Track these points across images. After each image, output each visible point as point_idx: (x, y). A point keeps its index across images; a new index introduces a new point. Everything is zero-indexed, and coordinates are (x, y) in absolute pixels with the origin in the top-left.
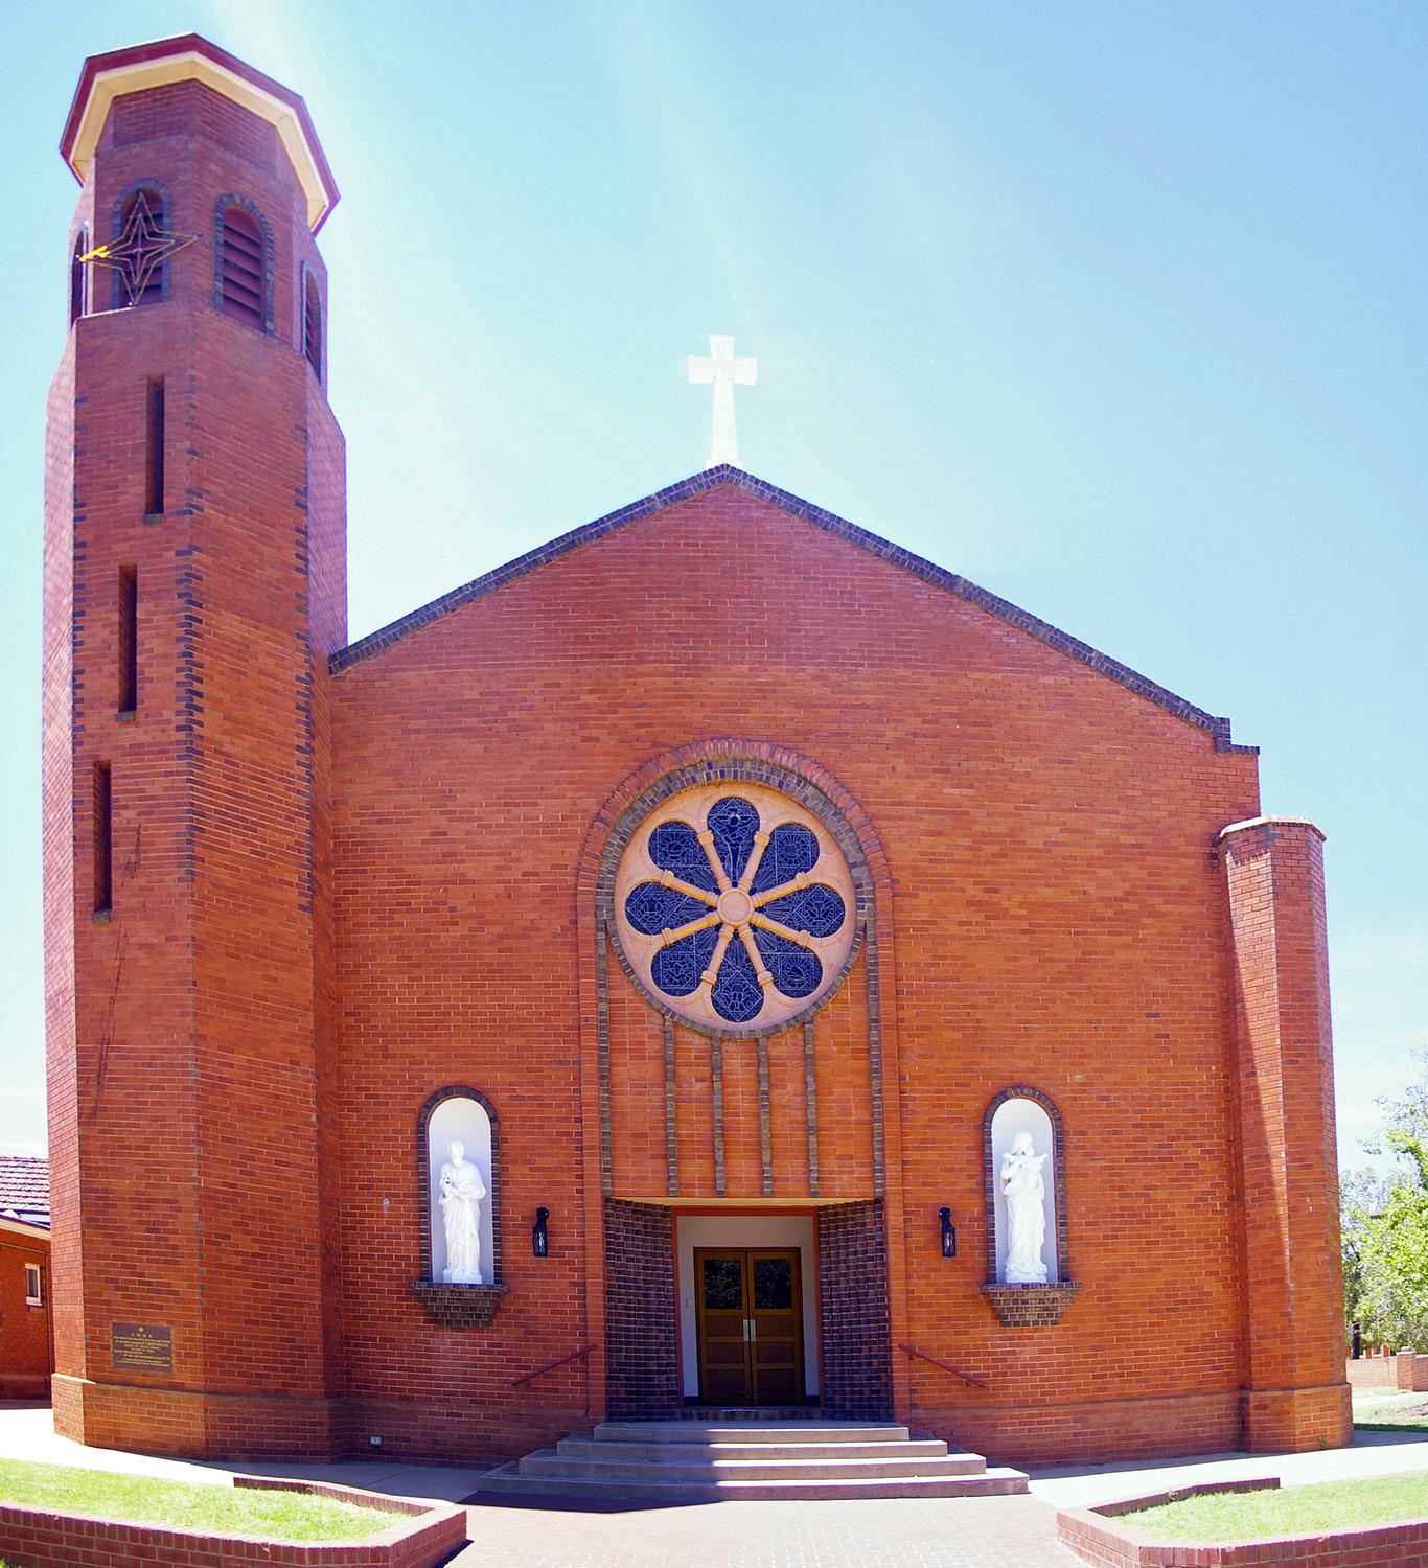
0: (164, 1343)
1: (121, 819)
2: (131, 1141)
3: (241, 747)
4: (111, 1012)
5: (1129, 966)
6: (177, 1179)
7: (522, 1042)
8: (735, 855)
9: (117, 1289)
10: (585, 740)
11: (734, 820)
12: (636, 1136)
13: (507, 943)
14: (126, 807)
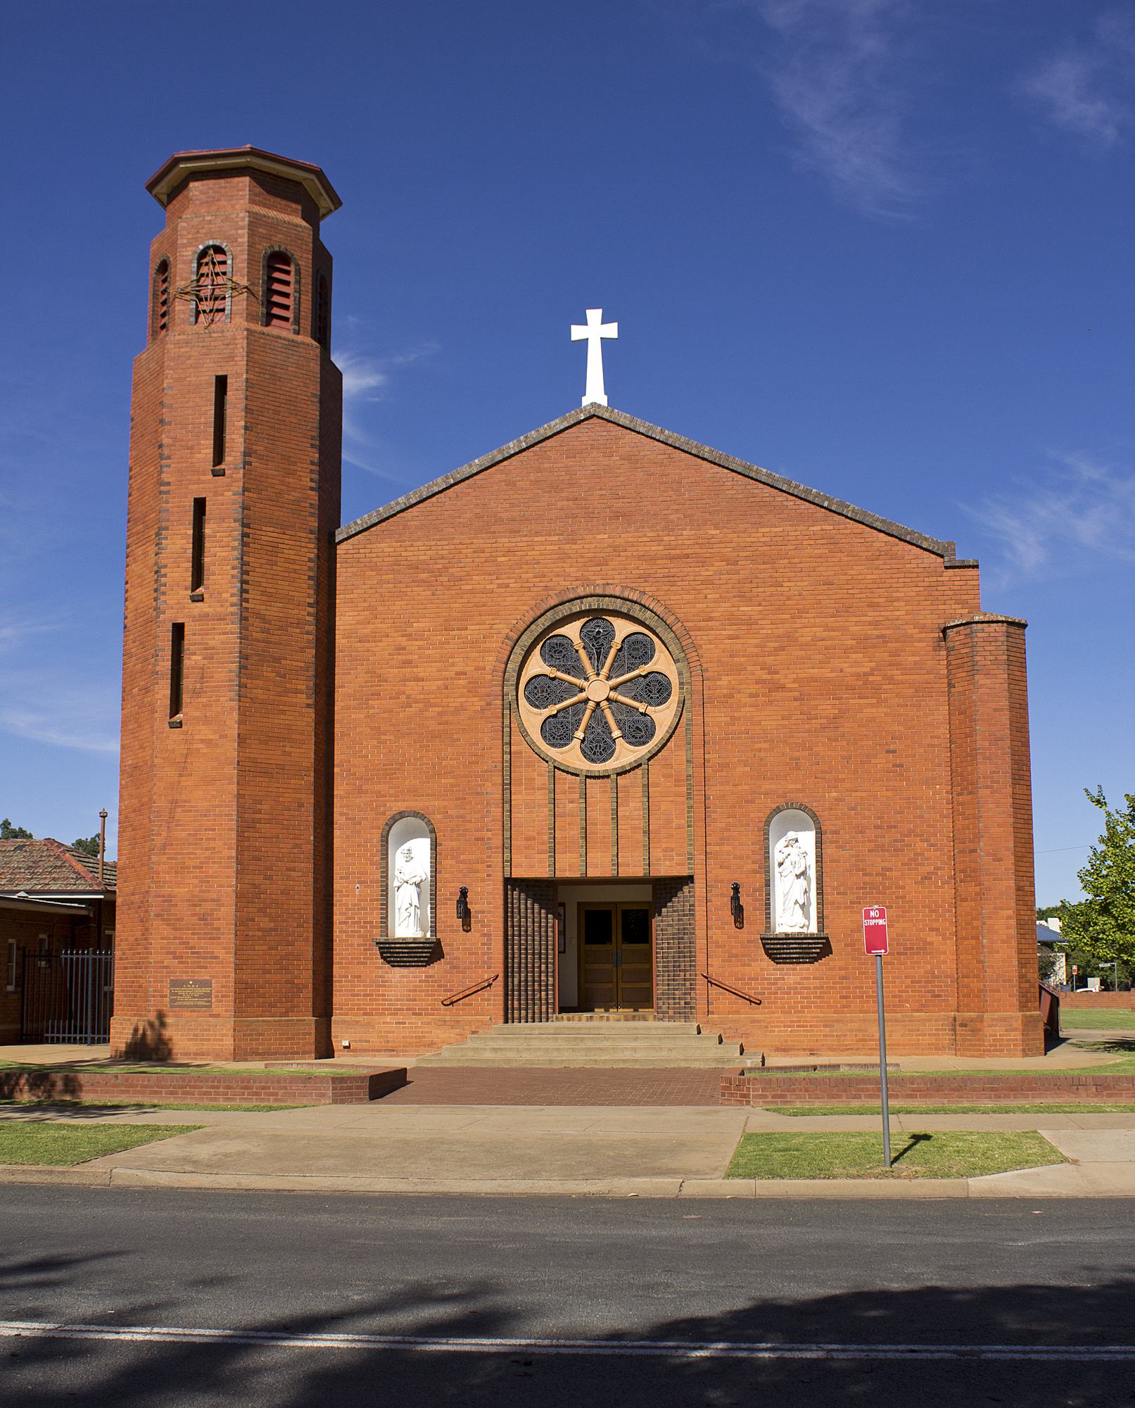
0: (207, 990)
1: (189, 662)
2: (188, 863)
4: (179, 782)
5: (872, 720)
6: (221, 886)
7: (452, 781)
8: (598, 656)
9: (175, 958)
10: (499, 586)
11: (599, 633)
12: (527, 839)
13: (444, 718)
14: (195, 654)
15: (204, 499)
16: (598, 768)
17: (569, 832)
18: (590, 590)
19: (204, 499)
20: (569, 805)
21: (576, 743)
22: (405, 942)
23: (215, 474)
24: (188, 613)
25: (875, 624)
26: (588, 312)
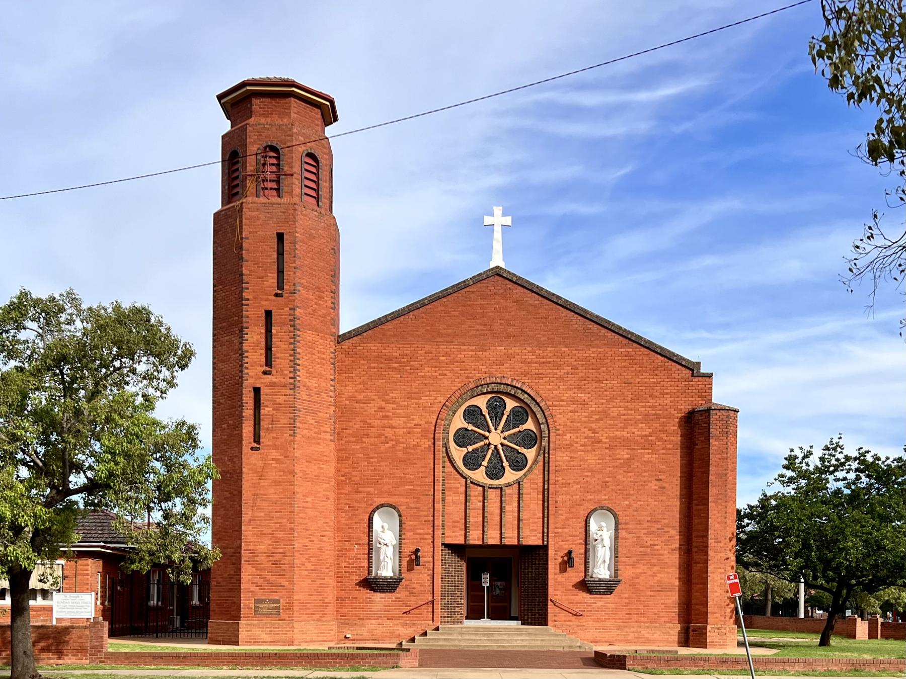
0: (277, 605)
3: (312, 383)
4: (259, 483)
5: (649, 461)
8: (497, 418)
12: (454, 522)
15: (271, 311)
16: (495, 483)
17: (475, 518)
18: (493, 380)
19: (271, 311)
20: (476, 502)
21: (482, 469)
22: (385, 578)
23: (276, 295)
24: (262, 382)
25: (653, 407)
26: (501, 208)
